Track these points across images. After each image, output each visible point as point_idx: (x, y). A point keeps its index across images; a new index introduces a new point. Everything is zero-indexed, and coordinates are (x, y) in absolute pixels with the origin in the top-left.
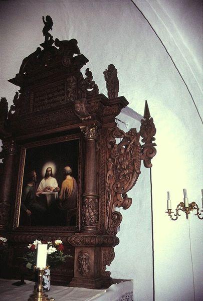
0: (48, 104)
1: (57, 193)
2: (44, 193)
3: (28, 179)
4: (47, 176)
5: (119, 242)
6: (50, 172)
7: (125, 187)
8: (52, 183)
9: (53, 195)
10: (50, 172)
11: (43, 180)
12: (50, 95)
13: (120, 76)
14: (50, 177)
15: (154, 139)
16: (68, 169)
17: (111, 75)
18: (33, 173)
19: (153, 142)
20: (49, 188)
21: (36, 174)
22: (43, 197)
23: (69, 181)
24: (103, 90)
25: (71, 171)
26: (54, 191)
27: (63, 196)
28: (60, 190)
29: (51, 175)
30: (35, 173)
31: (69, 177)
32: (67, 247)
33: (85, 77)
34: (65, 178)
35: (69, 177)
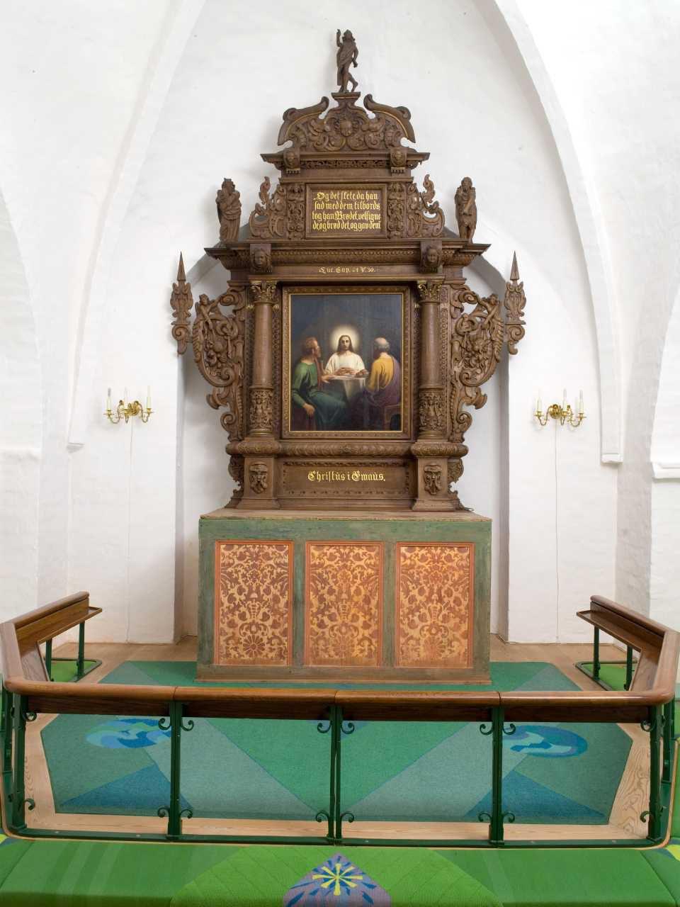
0: (346, 221)
1: (364, 379)
2: (337, 377)
3: (302, 352)
4: (341, 350)
5: (467, 178)
6: (347, 344)
7: (552, 409)
8: (354, 362)
9: (355, 383)
10: (347, 344)
11: (335, 357)
12: (350, 206)
13: (479, 201)
14: (348, 352)
15: (523, 314)
16: (383, 342)
17: (465, 193)
18: (314, 344)
19: (521, 318)
20: (348, 371)
21: (319, 345)
22: (335, 385)
23: (385, 363)
24: (451, 223)
25: (388, 346)
26: (358, 375)
27: (375, 385)
28: (370, 374)
29: (351, 349)
30: (316, 343)
31: (384, 356)
32: (312, 542)
33: (421, 189)
34: (377, 356)
35: (384, 356)
